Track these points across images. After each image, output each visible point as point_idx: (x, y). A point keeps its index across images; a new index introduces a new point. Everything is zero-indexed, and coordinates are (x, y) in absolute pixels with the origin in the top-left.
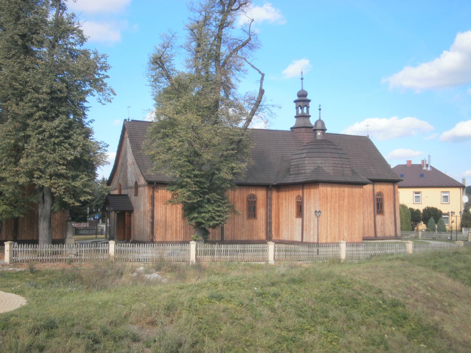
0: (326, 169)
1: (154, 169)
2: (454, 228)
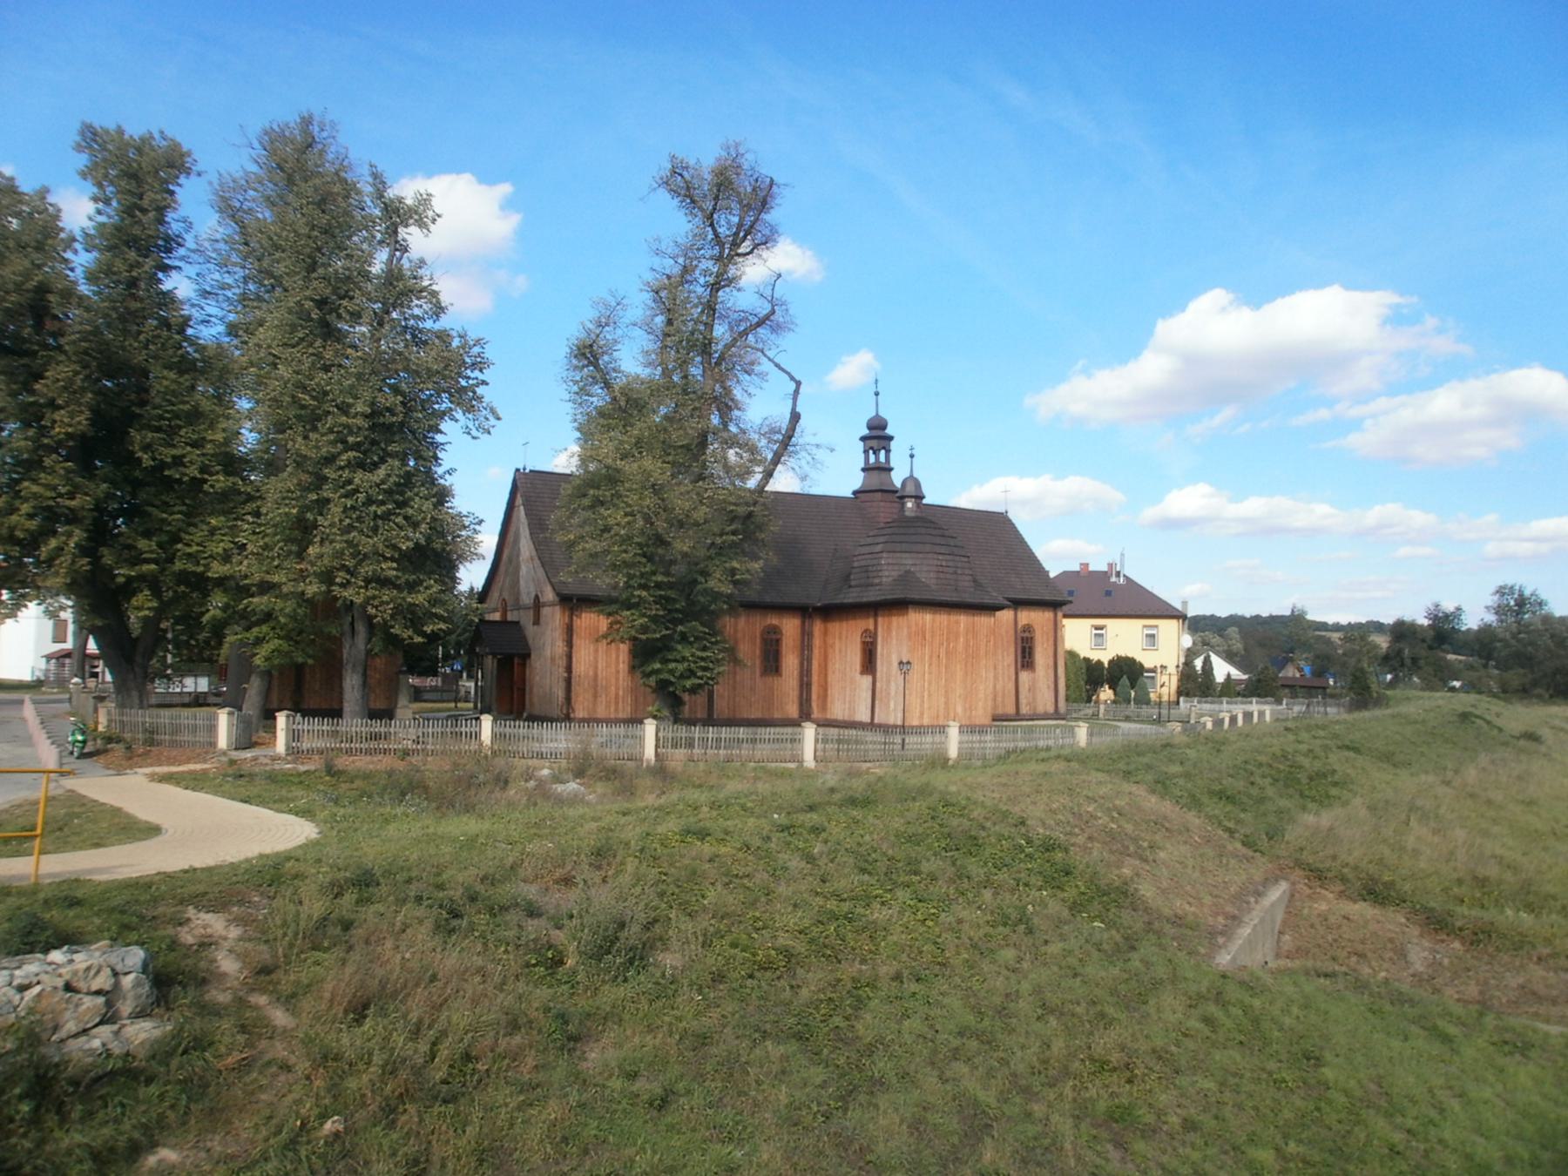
0: (923, 577)
1: (573, 568)
2: (1165, 698)
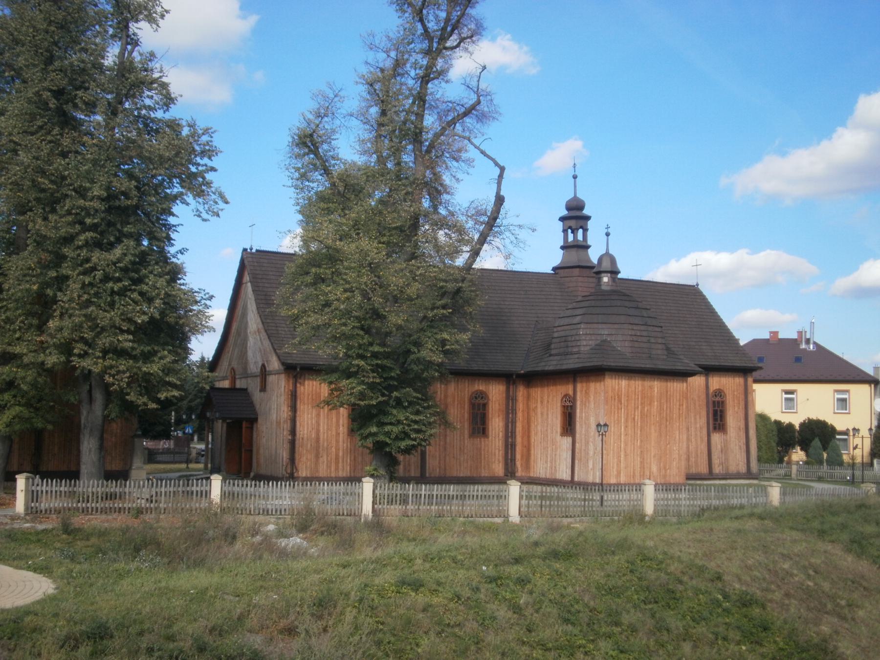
1: (296, 341)
2: (859, 460)
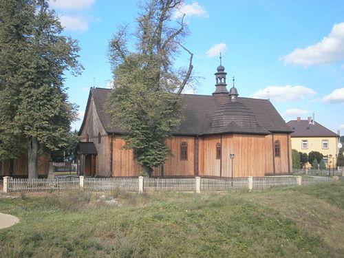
2: (332, 167)
